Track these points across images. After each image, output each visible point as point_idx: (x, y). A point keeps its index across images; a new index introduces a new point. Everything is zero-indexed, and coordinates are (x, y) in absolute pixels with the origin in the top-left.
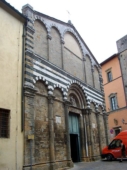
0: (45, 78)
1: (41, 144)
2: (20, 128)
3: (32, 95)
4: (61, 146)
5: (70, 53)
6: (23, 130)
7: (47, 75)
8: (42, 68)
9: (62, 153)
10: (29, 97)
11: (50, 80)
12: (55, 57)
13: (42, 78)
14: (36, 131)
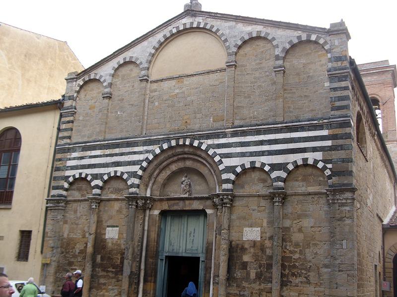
0: (85, 172)
2: (39, 250)
4: (110, 277)
5: (173, 82)
6: (42, 252)
7: (262, 153)
8: (82, 158)
9: (113, 289)
12: (79, 128)
13: (116, 172)
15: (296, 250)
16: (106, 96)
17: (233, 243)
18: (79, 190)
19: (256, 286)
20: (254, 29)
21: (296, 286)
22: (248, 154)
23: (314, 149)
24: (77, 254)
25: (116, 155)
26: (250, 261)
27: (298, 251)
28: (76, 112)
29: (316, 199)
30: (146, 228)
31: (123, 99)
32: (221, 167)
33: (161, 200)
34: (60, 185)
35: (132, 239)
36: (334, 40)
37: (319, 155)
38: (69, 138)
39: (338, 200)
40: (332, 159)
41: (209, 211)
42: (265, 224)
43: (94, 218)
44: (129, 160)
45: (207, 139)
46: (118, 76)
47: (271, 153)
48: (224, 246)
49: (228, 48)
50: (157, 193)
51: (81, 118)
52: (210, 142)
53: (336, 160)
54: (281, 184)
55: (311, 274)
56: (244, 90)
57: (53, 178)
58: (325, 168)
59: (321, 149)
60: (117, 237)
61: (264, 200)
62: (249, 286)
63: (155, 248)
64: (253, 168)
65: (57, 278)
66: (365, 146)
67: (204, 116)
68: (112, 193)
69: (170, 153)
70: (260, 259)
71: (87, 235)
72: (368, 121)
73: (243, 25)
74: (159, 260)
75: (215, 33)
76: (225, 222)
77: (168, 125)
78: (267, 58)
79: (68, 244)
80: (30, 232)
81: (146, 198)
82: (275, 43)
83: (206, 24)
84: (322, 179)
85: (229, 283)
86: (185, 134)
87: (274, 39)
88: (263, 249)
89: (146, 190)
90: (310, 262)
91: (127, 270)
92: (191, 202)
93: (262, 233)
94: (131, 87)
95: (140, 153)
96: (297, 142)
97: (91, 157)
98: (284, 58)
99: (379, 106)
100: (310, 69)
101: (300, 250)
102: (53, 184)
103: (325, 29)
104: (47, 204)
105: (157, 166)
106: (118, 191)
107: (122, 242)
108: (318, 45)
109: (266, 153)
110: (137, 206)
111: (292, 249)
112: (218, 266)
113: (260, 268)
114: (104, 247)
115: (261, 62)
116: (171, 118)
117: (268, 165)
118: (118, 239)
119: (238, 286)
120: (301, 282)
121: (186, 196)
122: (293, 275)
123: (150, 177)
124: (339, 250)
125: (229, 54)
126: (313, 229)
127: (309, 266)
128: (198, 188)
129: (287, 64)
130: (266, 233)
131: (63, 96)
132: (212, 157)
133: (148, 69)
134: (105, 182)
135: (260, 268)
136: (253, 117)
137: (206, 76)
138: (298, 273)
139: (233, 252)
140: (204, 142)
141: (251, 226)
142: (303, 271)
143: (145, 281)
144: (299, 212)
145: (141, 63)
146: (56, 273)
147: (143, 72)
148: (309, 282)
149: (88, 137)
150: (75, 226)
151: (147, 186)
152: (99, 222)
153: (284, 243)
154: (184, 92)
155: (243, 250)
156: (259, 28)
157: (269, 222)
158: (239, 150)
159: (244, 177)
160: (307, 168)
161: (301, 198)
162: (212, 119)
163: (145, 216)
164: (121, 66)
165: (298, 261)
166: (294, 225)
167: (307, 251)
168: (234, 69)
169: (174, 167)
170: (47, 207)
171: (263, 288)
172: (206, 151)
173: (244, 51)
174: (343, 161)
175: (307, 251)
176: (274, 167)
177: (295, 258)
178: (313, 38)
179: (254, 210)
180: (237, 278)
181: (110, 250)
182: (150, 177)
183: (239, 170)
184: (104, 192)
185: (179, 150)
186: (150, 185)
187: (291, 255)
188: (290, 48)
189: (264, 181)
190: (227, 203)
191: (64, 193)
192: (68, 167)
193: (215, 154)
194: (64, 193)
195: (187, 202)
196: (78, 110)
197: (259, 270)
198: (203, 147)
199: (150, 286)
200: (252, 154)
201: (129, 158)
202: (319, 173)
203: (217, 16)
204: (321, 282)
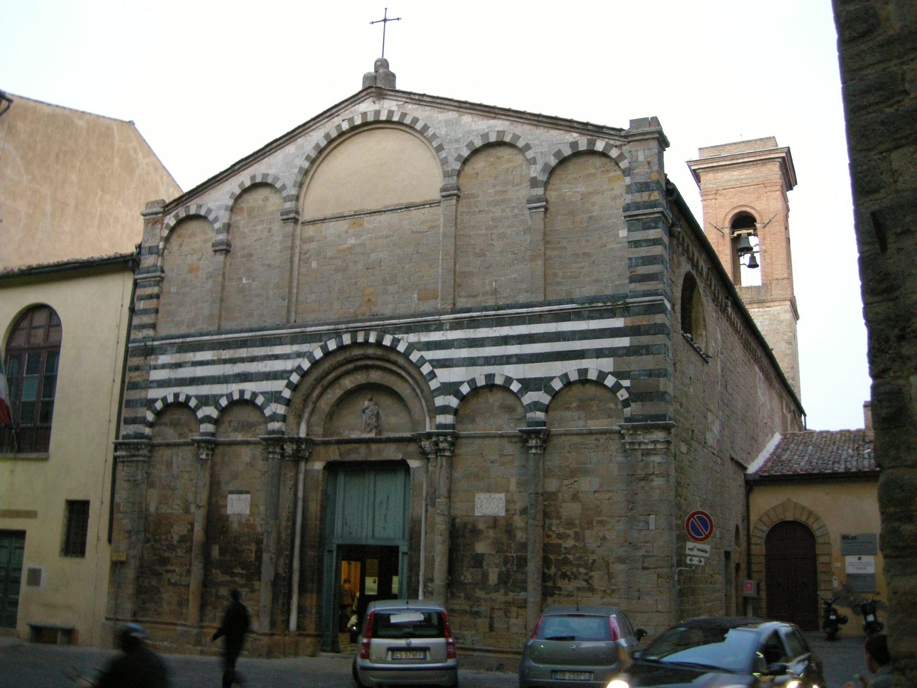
1: (169, 575)
2: (104, 535)
3: (133, 456)
5: (344, 225)
7: (507, 360)
8: (179, 365)
10: (128, 461)
11: (192, 390)
13: (242, 392)
14: (156, 541)
16: (220, 247)
17: (458, 520)
18: (175, 424)
19: (500, 597)
20: (495, 127)
21: (568, 595)
23: (599, 353)
24: (175, 543)
27: (572, 535)
28: (163, 278)
29: (602, 441)
30: (300, 494)
31: (251, 255)
32: (434, 384)
33: (326, 443)
34: (140, 415)
35: (276, 516)
36: (637, 151)
37: (607, 364)
38: (154, 326)
39: (640, 443)
41: (414, 464)
42: (513, 486)
43: (206, 477)
44: (267, 369)
46: (242, 209)
48: (441, 525)
49: (444, 162)
50: (320, 430)
52: (413, 338)
53: (637, 373)
54: (540, 415)
55: (596, 574)
58: (617, 387)
60: (247, 512)
62: (488, 596)
63: (318, 531)
64: (490, 386)
65: (141, 586)
67: (401, 290)
68: (235, 430)
69: (341, 357)
71: (193, 508)
74: (326, 553)
75: (423, 131)
76: (442, 484)
81: (298, 441)
82: (530, 154)
84: (612, 405)
86: (368, 324)
87: (528, 147)
88: (509, 531)
89: (299, 425)
90: (593, 552)
91: (268, 572)
92: (382, 446)
93: (508, 502)
94: (266, 231)
95: (286, 357)
96: (569, 340)
97: (195, 364)
98: (546, 184)
99: (755, 229)
100: (594, 204)
101: (576, 532)
105: (318, 380)
106: (246, 427)
107: (258, 520)
110: (283, 456)
111: (561, 530)
112: (430, 563)
115: (506, 189)
116: (341, 291)
117: (519, 381)
118: (249, 516)
120: (578, 588)
121: (372, 435)
122: (564, 576)
123: (305, 401)
124: (643, 532)
125: (447, 175)
126: (596, 495)
127: (590, 561)
128: (393, 420)
129: (552, 195)
130: (515, 502)
132: (417, 366)
133: (297, 198)
137: (404, 214)
138: (572, 573)
140: (402, 339)
141: (488, 491)
142: (582, 570)
145: (284, 187)
146: (138, 578)
147: (289, 205)
148: (591, 589)
149: (188, 326)
150: (169, 492)
151: (300, 417)
152: (214, 486)
153: (547, 520)
154: (365, 245)
155: (475, 532)
157: (519, 484)
158: (464, 353)
159: (475, 401)
160: (587, 386)
161: (576, 439)
162: (416, 296)
163: (297, 473)
164: (246, 191)
166: (564, 489)
167: (588, 533)
168: (454, 202)
169: (348, 383)
171: (511, 600)
175: (588, 533)
176: (528, 384)
177: (566, 546)
178: (600, 146)
180: (466, 584)
182: (305, 401)
183: (465, 389)
184: (224, 427)
185: (357, 352)
186: (306, 415)
187: (560, 541)
189: (510, 409)
190: (444, 450)
191: (147, 431)
192: (152, 382)
193: (422, 361)
194: (147, 431)
195: (374, 447)
196: (169, 274)
197: (504, 569)
198: (401, 348)
199: (311, 600)
201: (265, 367)
202: (608, 395)
204: (613, 588)
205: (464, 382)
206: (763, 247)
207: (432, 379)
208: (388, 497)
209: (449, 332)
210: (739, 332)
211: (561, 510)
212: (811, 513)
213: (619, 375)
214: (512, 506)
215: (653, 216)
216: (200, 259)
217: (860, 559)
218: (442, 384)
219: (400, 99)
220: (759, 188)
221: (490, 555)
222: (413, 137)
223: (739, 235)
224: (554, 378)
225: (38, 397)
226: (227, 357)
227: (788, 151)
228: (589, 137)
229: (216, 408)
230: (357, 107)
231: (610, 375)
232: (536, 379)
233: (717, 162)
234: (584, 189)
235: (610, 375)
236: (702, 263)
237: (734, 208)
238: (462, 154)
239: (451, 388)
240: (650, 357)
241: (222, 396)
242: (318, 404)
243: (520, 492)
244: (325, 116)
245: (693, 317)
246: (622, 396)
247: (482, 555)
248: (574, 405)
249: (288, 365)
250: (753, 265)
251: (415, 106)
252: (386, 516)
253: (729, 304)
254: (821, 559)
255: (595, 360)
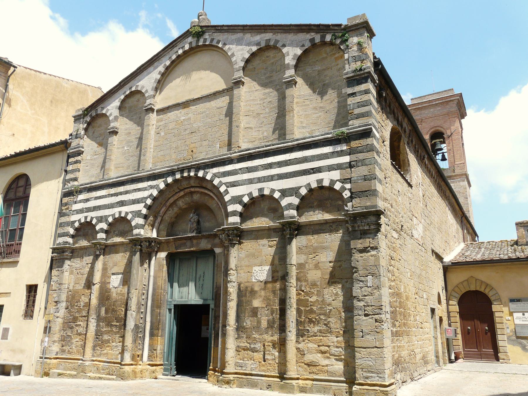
7: (271, 178)
8: (87, 200)
9: (116, 346)
15: (313, 290)
17: (242, 285)
22: (256, 181)
23: (330, 168)
25: (121, 193)
26: (260, 306)
37: (336, 175)
40: (351, 178)
41: (218, 250)
44: (134, 198)
45: (212, 168)
46: (125, 107)
47: (281, 177)
51: (89, 158)
52: (215, 170)
53: (355, 178)
56: (252, 109)
57: (60, 225)
58: (343, 189)
59: (339, 167)
61: (275, 233)
62: (261, 337)
66: (409, 169)
70: (272, 303)
72: (412, 141)
73: (251, 35)
77: (174, 156)
78: (277, 70)
79: (73, 297)
80: (36, 286)
83: (212, 40)
85: (238, 334)
90: (329, 305)
91: (131, 324)
94: (138, 118)
95: (144, 189)
96: (310, 162)
99: (444, 138)
100: (326, 76)
102: (61, 231)
103: (340, 25)
104: (52, 253)
108: (334, 46)
109: (276, 177)
113: (272, 314)
114: (108, 298)
115: (271, 75)
117: (279, 191)
119: (248, 337)
122: (311, 321)
127: (328, 311)
130: (278, 272)
131: (71, 135)
134: (110, 225)
135: (272, 314)
136: (262, 138)
138: (316, 319)
139: (242, 297)
142: (322, 317)
143: (152, 335)
144: (316, 245)
155: (253, 292)
156: (268, 36)
162: (218, 145)
164: (127, 97)
165: (316, 305)
170: (52, 257)
172: (211, 181)
173: (253, 65)
174: (365, 178)
176: (284, 193)
179: (263, 246)
181: (114, 301)
187: (307, 297)
188: (302, 54)
192: (74, 211)
193: (221, 184)
200: (260, 180)
201: (133, 196)
203: (223, 30)
205: (246, 195)
206: (449, 148)
207: (227, 194)
208: (204, 273)
209: (236, 164)
210: (434, 178)
211: (308, 275)
212: (487, 285)
213: (344, 181)
214: (276, 274)
215: (364, 76)
216: (103, 139)
217: (524, 315)
218: (232, 197)
219: (210, 31)
220: (446, 116)
221: (262, 307)
222: (218, 53)
223: (435, 143)
224: (301, 187)
225: (18, 226)
226: (113, 192)
227: (461, 95)
228: (322, 34)
229: (106, 223)
230: (186, 40)
231: (338, 182)
232: (290, 189)
233: (422, 105)
234: (320, 68)
235: (338, 182)
236: (405, 125)
237: (432, 129)
238: (245, 56)
239: (237, 200)
240: (364, 167)
241: (109, 216)
242: (164, 217)
243: (281, 265)
244: (169, 47)
245: (401, 159)
246: (346, 195)
247: (257, 308)
248: (315, 204)
249: (146, 194)
250: (444, 159)
251: (218, 34)
252: (203, 285)
253: (426, 156)
254: (497, 314)
255: (328, 172)
